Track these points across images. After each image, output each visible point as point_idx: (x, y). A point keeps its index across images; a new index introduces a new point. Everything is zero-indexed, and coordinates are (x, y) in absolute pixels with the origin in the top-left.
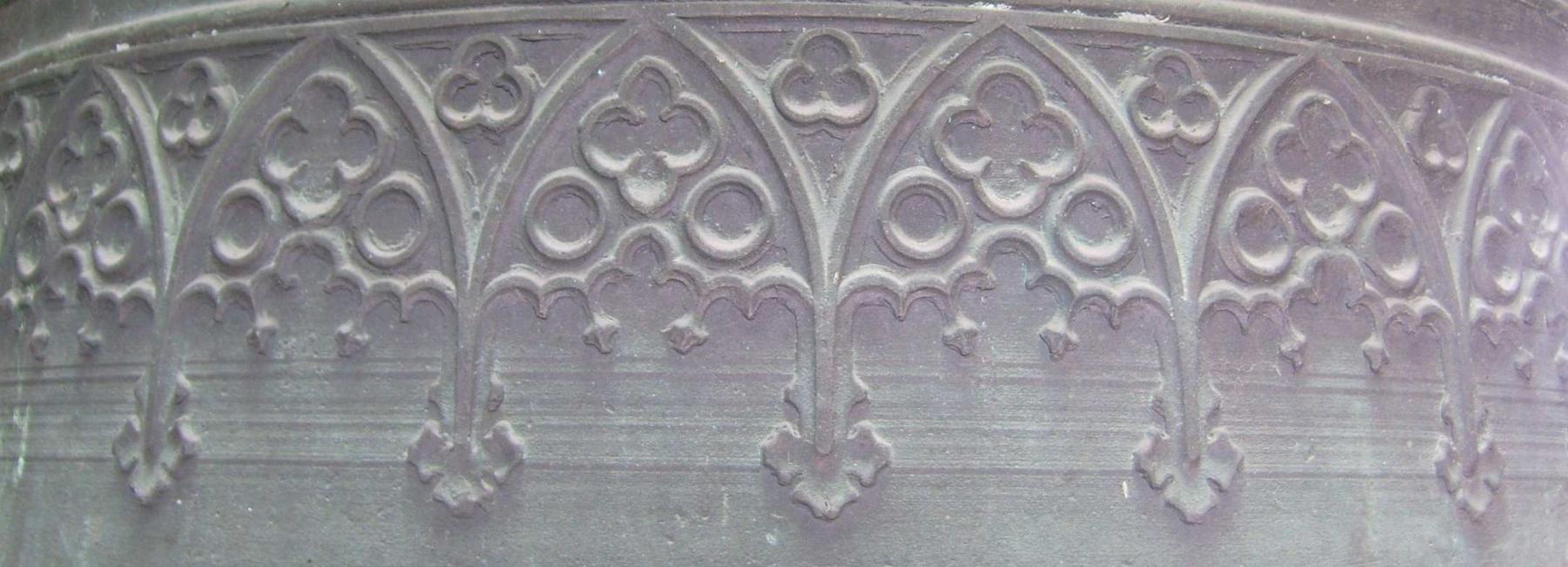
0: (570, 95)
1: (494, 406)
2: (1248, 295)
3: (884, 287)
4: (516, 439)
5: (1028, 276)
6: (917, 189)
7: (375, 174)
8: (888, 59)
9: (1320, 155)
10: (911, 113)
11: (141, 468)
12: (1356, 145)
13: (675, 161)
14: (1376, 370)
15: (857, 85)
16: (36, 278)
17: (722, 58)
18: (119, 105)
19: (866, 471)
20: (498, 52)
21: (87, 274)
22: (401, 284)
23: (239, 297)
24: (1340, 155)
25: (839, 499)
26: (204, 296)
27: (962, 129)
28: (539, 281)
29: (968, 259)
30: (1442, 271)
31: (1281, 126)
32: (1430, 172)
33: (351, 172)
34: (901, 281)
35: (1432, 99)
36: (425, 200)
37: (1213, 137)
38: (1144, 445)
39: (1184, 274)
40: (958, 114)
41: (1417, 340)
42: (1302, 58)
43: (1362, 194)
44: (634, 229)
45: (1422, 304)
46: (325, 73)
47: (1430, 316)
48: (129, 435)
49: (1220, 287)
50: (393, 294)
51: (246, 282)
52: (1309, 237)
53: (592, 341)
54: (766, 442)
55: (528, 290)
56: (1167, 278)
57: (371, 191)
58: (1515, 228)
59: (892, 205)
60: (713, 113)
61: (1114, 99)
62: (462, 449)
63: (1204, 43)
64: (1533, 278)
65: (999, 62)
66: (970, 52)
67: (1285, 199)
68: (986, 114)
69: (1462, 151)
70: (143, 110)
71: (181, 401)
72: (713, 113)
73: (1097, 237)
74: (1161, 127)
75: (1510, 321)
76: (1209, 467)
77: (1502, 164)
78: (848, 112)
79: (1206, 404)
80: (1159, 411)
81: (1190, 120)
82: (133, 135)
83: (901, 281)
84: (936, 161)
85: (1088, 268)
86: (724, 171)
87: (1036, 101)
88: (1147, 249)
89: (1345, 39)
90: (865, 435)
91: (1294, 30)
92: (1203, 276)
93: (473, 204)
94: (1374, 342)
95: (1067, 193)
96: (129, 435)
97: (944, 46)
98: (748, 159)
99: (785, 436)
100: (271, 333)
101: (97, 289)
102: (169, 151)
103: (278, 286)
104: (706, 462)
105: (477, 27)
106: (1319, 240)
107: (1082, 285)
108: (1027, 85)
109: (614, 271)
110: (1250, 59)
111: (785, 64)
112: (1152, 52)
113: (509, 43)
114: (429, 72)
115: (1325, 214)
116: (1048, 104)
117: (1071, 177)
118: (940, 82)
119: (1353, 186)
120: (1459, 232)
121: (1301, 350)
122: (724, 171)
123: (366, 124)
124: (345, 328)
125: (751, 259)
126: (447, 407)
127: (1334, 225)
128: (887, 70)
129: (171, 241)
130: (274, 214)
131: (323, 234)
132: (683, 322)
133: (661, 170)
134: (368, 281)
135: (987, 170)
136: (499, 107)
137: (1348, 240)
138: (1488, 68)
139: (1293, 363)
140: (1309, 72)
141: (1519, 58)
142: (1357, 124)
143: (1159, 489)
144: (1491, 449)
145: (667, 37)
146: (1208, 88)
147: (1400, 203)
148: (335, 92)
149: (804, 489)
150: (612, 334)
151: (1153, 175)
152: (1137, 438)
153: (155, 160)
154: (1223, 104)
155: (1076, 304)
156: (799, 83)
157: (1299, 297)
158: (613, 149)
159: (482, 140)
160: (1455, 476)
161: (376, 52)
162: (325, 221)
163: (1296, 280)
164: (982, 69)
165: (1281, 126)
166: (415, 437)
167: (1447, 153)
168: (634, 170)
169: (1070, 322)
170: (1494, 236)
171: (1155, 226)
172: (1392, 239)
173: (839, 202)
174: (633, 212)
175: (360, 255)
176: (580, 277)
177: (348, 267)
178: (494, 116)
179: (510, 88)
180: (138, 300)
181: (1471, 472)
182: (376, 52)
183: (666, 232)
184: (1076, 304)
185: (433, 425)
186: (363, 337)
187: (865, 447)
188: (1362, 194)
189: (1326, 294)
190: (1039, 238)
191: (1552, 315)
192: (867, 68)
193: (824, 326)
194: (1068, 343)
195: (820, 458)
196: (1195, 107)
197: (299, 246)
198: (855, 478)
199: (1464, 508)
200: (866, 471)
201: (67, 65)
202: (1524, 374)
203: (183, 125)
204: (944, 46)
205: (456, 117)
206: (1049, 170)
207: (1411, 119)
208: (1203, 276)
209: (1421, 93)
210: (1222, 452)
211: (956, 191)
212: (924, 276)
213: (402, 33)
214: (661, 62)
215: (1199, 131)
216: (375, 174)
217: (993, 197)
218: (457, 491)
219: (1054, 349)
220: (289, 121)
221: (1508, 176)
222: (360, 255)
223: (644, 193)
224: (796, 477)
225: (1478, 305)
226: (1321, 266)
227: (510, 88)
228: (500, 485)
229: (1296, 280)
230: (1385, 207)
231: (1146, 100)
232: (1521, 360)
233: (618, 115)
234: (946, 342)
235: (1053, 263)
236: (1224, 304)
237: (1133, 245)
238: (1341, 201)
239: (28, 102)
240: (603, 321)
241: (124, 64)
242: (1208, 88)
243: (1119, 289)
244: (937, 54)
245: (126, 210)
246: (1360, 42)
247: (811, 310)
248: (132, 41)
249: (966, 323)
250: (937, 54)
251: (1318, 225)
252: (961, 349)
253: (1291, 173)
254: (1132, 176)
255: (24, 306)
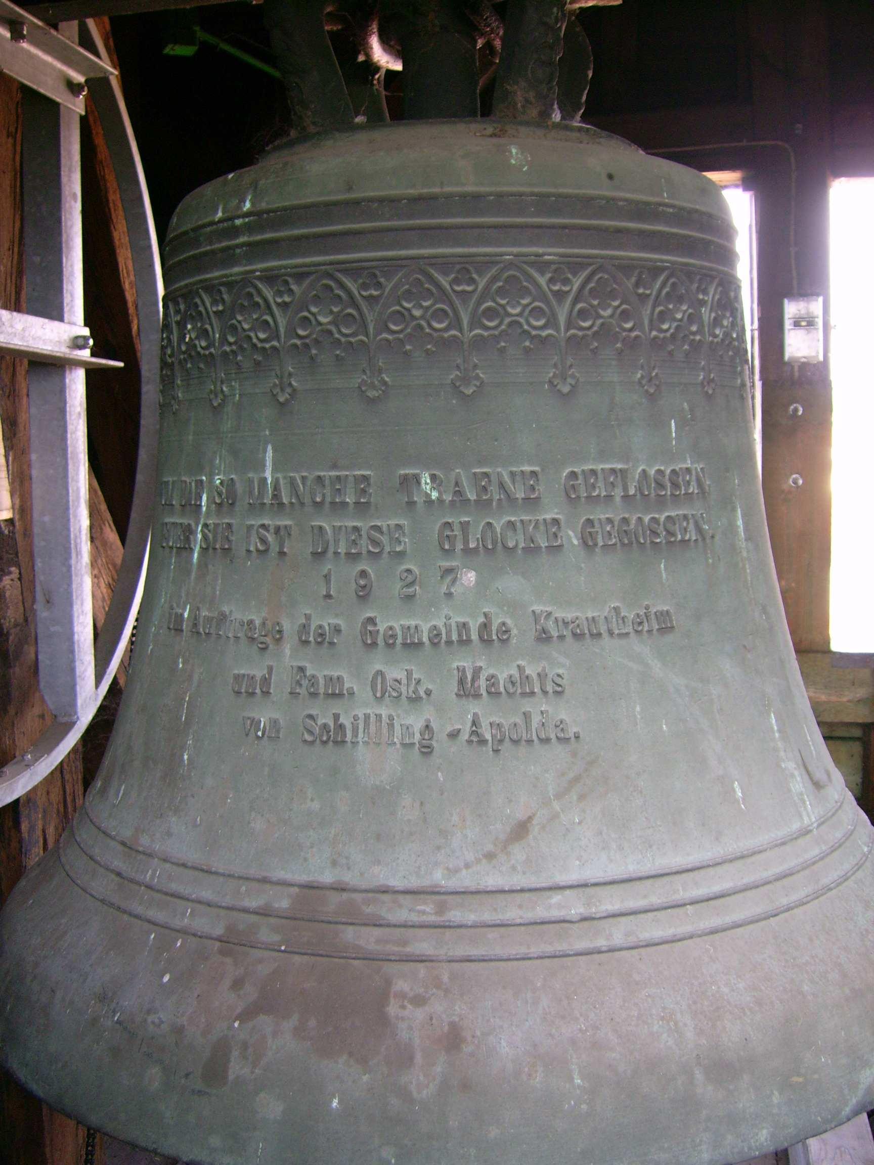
0: (396, 287)
1: (380, 371)
2: (580, 333)
3: (482, 336)
4: (387, 379)
5: (519, 331)
6: (489, 309)
7: (342, 310)
8: (480, 274)
9: (604, 293)
10: (487, 287)
11: (280, 394)
12: (615, 289)
13: (425, 304)
14: (620, 352)
15: (472, 281)
16: (235, 343)
17: (436, 275)
18: (259, 292)
19: (478, 384)
20: (375, 276)
21: (255, 340)
22: (352, 340)
23: (306, 346)
24: (611, 292)
25: (471, 391)
26: (295, 346)
27: (501, 292)
28: (390, 337)
29: (503, 327)
30: (642, 324)
31: (592, 285)
32: (640, 295)
33: (335, 310)
34: (486, 334)
35: (641, 273)
36: (357, 316)
37: (571, 290)
38: (551, 374)
39: (562, 328)
40: (500, 287)
41: (633, 344)
42: (598, 265)
43: (616, 303)
44: (415, 323)
45: (698, 338)
46: (325, 282)
47: (637, 337)
48: (275, 385)
49: (572, 331)
50: (351, 343)
51: (307, 341)
52: (599, 316)
53: (406, 353)
54: (452, 377)
55: (387, 340)
56: (557, 330)
57: (342, 315)
58: (669, 310)
59: (92, 565)
60: (434, 290)
61: (542, 281)
62: (372, 383)
63: (569, 263)
64: (675, 324)
65: (511, 272)
66: (502, 270)
67: (592, 306)
68: (508, 287)
69: (651, 288)
70: (268, 293)
71: (290, 375)
72: (434, 290)
73: (538, 320)
74: (556, 288)
75: (717, 342)
76: (569, 380)
77: (667, 290)
78: (469, 288)
79: (569, 363)
80: (555, 366)
81: (564, 286)
82: (266, 300)
83: (486, 334)
84: (494, 301)
85: (535, 328)
86: (438, 306)
87: (521, 282)
88: (552, 322)
89: (612, 258)
90: (477, 374)
91: (596, 257)
92: (567, 329)
93: (370, 317)
94: (619, 345)
95: (530, 308)
96: (275, 385)
97: (495, 269)
98: (443, 302)
99: (457, 375)
100: (316, 355)
101: (259, 345)
102: (278, 305)
103: (317, 341)
104: (437, 383)
105: (368, 268)
106: (602, 317)
107: (534, 333)
108: (519, 278)
109: (410, 334)
110: (582, 266)
111: (453, 276)
112: (553, 267)
113: (378, 273)
114: (355, 281)
115: (605, 309)
116: (525, 284)
117: (530, 304)
118: (494, 279)
119: (613, 301)
120: (648, 312)
121: (596, 348)
122: (438, 306)
123: (339, 297)
124: (338, 352)
125: (446, 330)
126: (368, 372)
127: (608, 312)
128: (480, 276)
129: (282, 330)
130: (314, 322)
131: (329, 327)
132: (429, 347)
133: (421, 307)
134: (343, 340)
135: (508, 303)
136: (376, 290)
137: (612, 316)
138: (662, 261)
139: (594, 351)
140: (601, 268)
141: (673, 256)
142: (617, 283)
143: (556, 386)
144: (657, 375)
145: (420, 269)
146: (570, 276)
147: (629, 305)
148: (328, 288)
149: (462, 389)
150: (410, 351)
151: (554, 302)
152: (549, 373)
153: (274, 307)
154: (574, 280)
155: (533, 338)
156: (456, 281)
157: (595, 334)
158: (409, 301)
159: (371, 299)
160: (644, 382)
161: (339, 275)
162: (329, 323)
163: (595, 328)
164: (506, 275)
165: (592, 285)
166: (360, 380)
167: (645, 288)
168: (414, 307)
169: (531, 343)
170: (661, 312)
171: (554, 315)
172: (625, 315)
173: (470, 309)
174: (413, 318)
175: (340, 332)
176: (401, 336)
177: (337, 336)
178: (375, 293)
179: (379, 285)
180: (274, 348)
181: (650, 380)
182: (339, 275)
183: (423, 323)
184: (533, 338)
185: (365, 377)
186: (343, 354)
187: (477, 377)
188: (616, 303)
189: (605, 333)
190: (522, 320)
191: (682, 335)
192: (475, 276)
193: (466, 346)
194: (530, 349)
195: (466, 380)
196: (566, 281)
197: (322, 331)
198: (475, 386)
199: (647, 391)
200: (478, 384)
201: (239, 278)
202: (670, 353)
203: (281, 296)
204: (495, 269)
205: (364, 293)
206: (524, 302)
207: (633, 279)
208: (567, 329)
209: (636, 273)
210: (573, 376)
211: (500, 309)
212: (492, 332)
213: (346, 270)
214: (420, 277)
215: (566, 289)
216: (342, 310)
217: (510, 310)
218: (372, 394)
219: (527, 351)
220: (315, 295)
221: (668, 294)
222: (340, 332)
223: (417, 313)
224: (460, 386)
225: (711, 339)
226: (603, 324)
227: (379, 285)
228: (383, 391)
229: (595, 328)
230: (624, 306)
231: (551, 281)
232: (669, 349)
233: (408, 292)
234: (498, 349)
235: (526, 327)
236: (574, 336)
237: (548, 321)
238: (610, 305)
239: (223, 289)
240: (408, 347)
241: (259, 278)
242: (570, 276)
243: (544, 333)
244: (494, 271)
245: (266, 322)
246: (617, 258)
247: (462, 342)
248: (261, 272)
249: (503, 344)
250: (494, 271)
251: (602, 313)
252: (502, 350)
253: (595, 298)
254: (548, 303)
255: (184, 359)
